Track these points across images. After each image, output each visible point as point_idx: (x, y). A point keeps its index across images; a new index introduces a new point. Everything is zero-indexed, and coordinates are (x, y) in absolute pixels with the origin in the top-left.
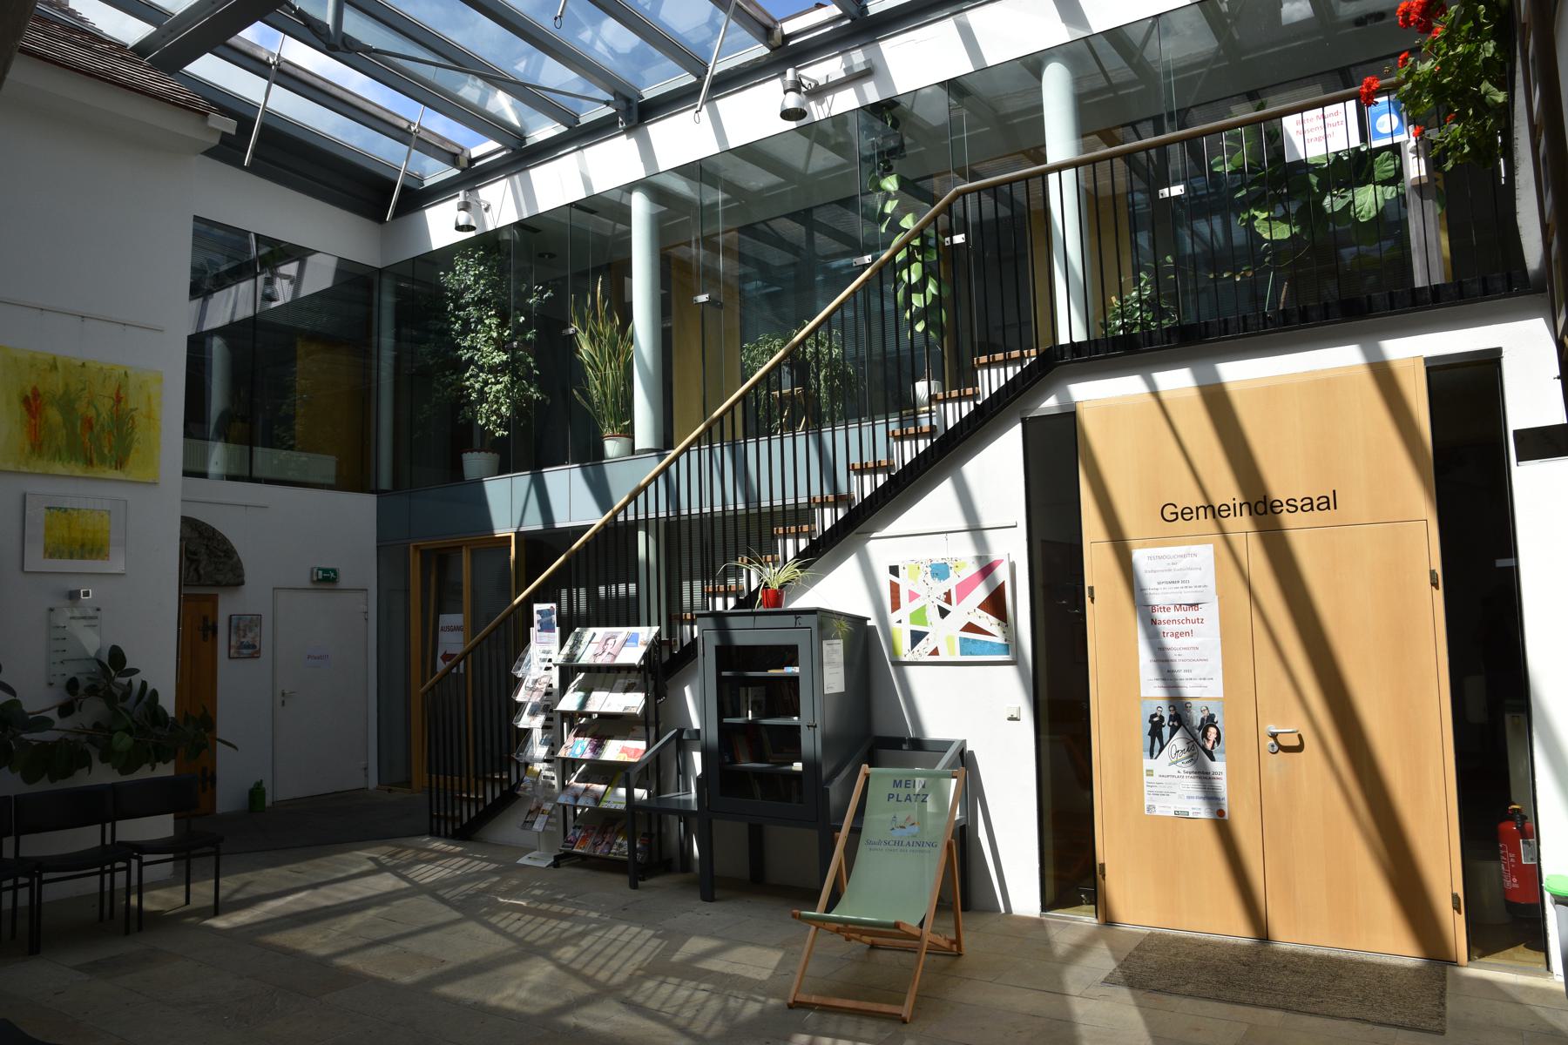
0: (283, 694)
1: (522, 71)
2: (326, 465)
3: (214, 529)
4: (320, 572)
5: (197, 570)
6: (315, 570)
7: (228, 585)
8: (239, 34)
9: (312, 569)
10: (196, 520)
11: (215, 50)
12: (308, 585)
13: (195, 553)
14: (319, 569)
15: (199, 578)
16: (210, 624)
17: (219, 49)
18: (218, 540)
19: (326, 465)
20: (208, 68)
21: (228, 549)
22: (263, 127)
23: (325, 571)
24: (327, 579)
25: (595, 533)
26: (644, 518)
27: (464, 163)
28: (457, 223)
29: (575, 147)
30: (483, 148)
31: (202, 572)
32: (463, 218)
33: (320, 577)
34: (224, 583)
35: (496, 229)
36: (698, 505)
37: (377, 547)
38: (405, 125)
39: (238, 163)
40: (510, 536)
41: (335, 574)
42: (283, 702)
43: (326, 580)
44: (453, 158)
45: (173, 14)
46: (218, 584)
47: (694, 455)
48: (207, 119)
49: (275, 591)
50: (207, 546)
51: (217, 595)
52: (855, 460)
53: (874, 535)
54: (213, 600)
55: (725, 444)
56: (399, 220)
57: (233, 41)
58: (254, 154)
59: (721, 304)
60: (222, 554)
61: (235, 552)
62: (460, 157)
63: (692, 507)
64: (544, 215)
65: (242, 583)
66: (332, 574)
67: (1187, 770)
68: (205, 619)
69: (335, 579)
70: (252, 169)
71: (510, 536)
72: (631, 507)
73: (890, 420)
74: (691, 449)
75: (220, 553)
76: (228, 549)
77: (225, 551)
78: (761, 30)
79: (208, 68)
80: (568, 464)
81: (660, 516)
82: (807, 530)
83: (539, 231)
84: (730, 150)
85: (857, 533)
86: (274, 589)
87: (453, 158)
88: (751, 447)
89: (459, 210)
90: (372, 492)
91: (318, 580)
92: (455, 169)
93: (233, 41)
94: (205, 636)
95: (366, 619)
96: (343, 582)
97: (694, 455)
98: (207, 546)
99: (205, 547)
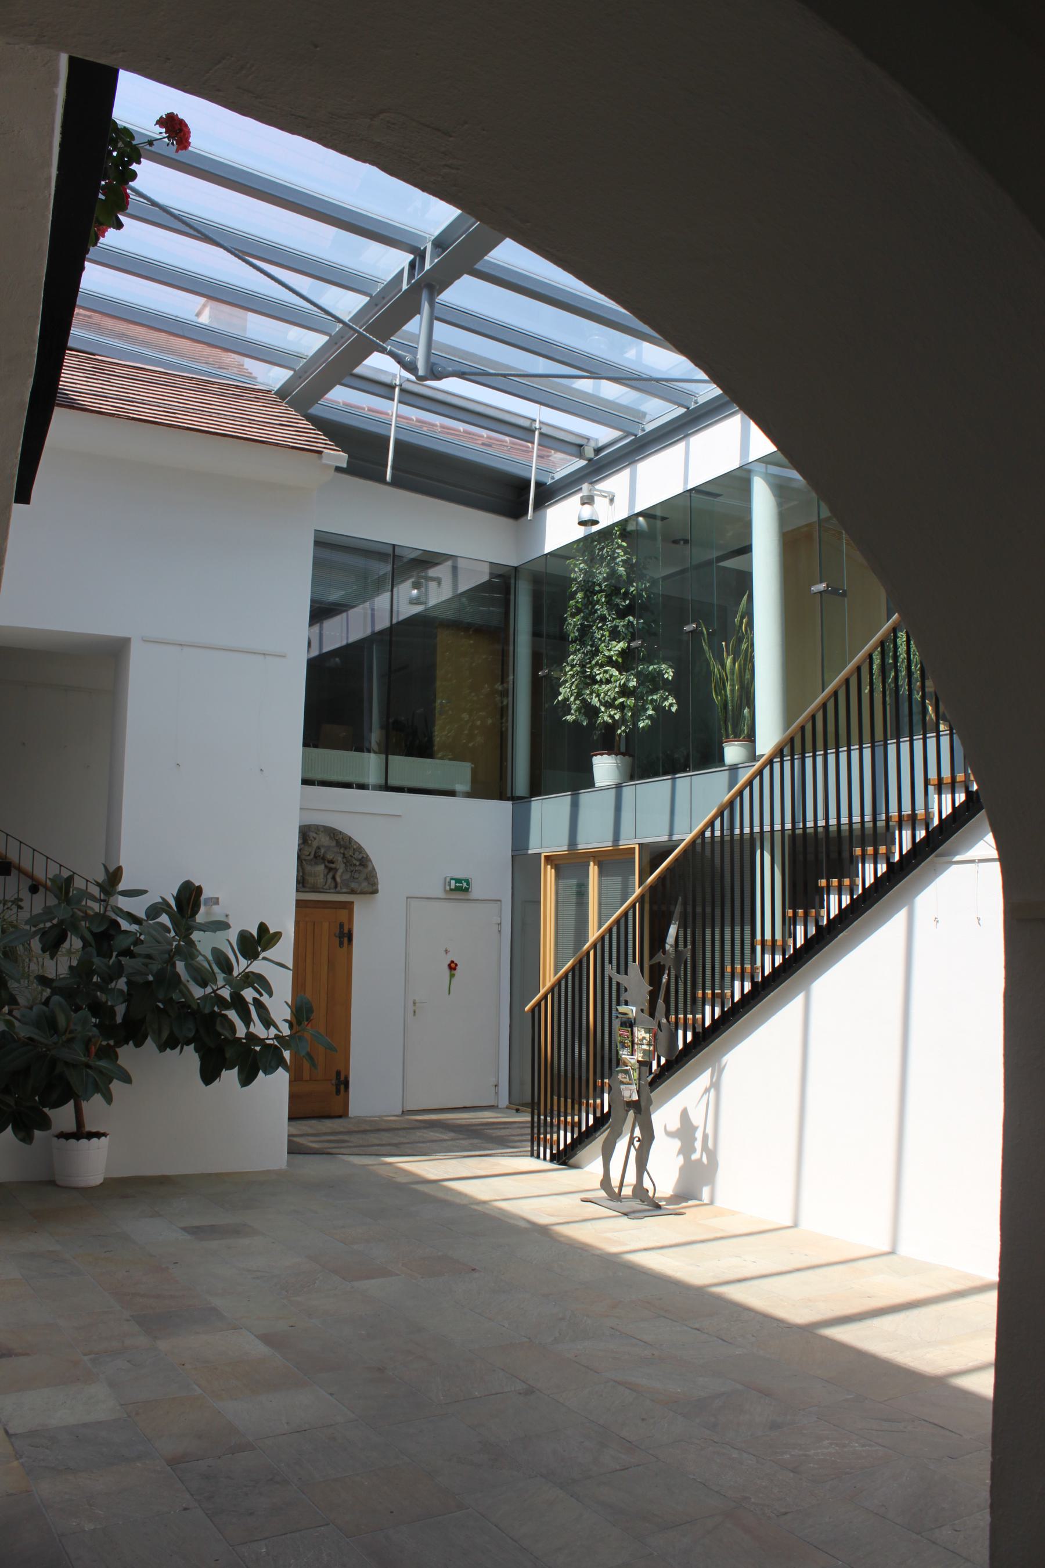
0: (414, 1003)
1: (634, 358)
2: (460, 774)
3: (350, 838)
4: (453, 882)
5: (334, 878)
6: (448, 879)
7: (362, 893)
8: (364, 363)
9: (445, 878)
10: (335, 829)
11: (343, 381)
12: (442, 895)
13: (332, 862)
14: (452, 879)
15: (336, 887)
16: (346, 931)
17: (348, 380)
18: (354, 849)
19: (460, 774)
20: (340, 396)
21: (363, 857)
22: (397, 442)
23: (458, 881)
24: (460, 888)
25: (685, 851)
26: (812, 825)
27: (589, 453)
28: (579, 518)
29: (627, 463)
30: (602, 434)
31: (338, 879)
32: (587, 513)
33: (453, 887)
34: (358, 892)
35: (348, 646)
36: (859, 813)
37: (512, 856)
38: (526, 423)
39: (382, 479)
40: (634, 848)
41: (468, 884)
42: (415, 1012)
43: (458, 889)
44: (578, 449)
45: (307, 356)
46: (353, 892)
47: (777, 767)
48: (322, 457)
49: (408, 899)
50: (344, 854)
51: (352, 903)
52: (933, 775)
53: (957, 858)
54: (349, 906)
55: (796, 757)
56: (539, 513)
57: (358, 370)
58: (393, 468)
59: (844, 591)
60: (358, 863)
61: (370, 860)
62: (586, 448)
63: (854, 815)
64: (733, 473)
65: (375, 892)
66: (465, 885)
67: (16, 985)
68: (342, 926)
69: (468, 889)
70: (396, 483)
71: (634, 848)
72: (718, 823)
73: (852, 748)
74: (775, 760)
75: (355, 862)
76: (363, 857)
77: (360, 860)
78: (574, 450)
79: (340, 396)
80: (689, 771)
81: (786, 828)
82: (884, 851)
83: (667, 518)
84: (688, 490)
85: (936, 856)
86: (407, 898)
87: (578, 449)
88: (892, 749)
89: (583, 504)
90: (508, 799)
91: (451, 890)
92: (581, 460)
93: (358, 370)
94: (341, 944)
95: (500, 931)
96: (476, 892)
97: (777, 767)
98: (344, 854)
99: (342, 855)
